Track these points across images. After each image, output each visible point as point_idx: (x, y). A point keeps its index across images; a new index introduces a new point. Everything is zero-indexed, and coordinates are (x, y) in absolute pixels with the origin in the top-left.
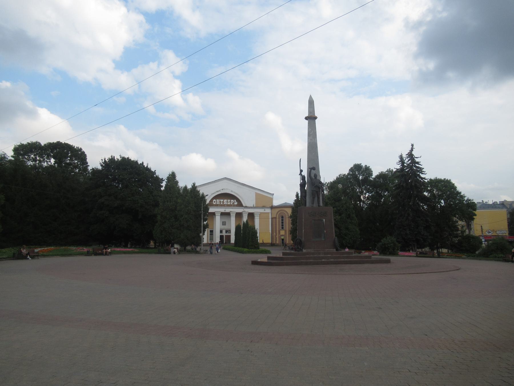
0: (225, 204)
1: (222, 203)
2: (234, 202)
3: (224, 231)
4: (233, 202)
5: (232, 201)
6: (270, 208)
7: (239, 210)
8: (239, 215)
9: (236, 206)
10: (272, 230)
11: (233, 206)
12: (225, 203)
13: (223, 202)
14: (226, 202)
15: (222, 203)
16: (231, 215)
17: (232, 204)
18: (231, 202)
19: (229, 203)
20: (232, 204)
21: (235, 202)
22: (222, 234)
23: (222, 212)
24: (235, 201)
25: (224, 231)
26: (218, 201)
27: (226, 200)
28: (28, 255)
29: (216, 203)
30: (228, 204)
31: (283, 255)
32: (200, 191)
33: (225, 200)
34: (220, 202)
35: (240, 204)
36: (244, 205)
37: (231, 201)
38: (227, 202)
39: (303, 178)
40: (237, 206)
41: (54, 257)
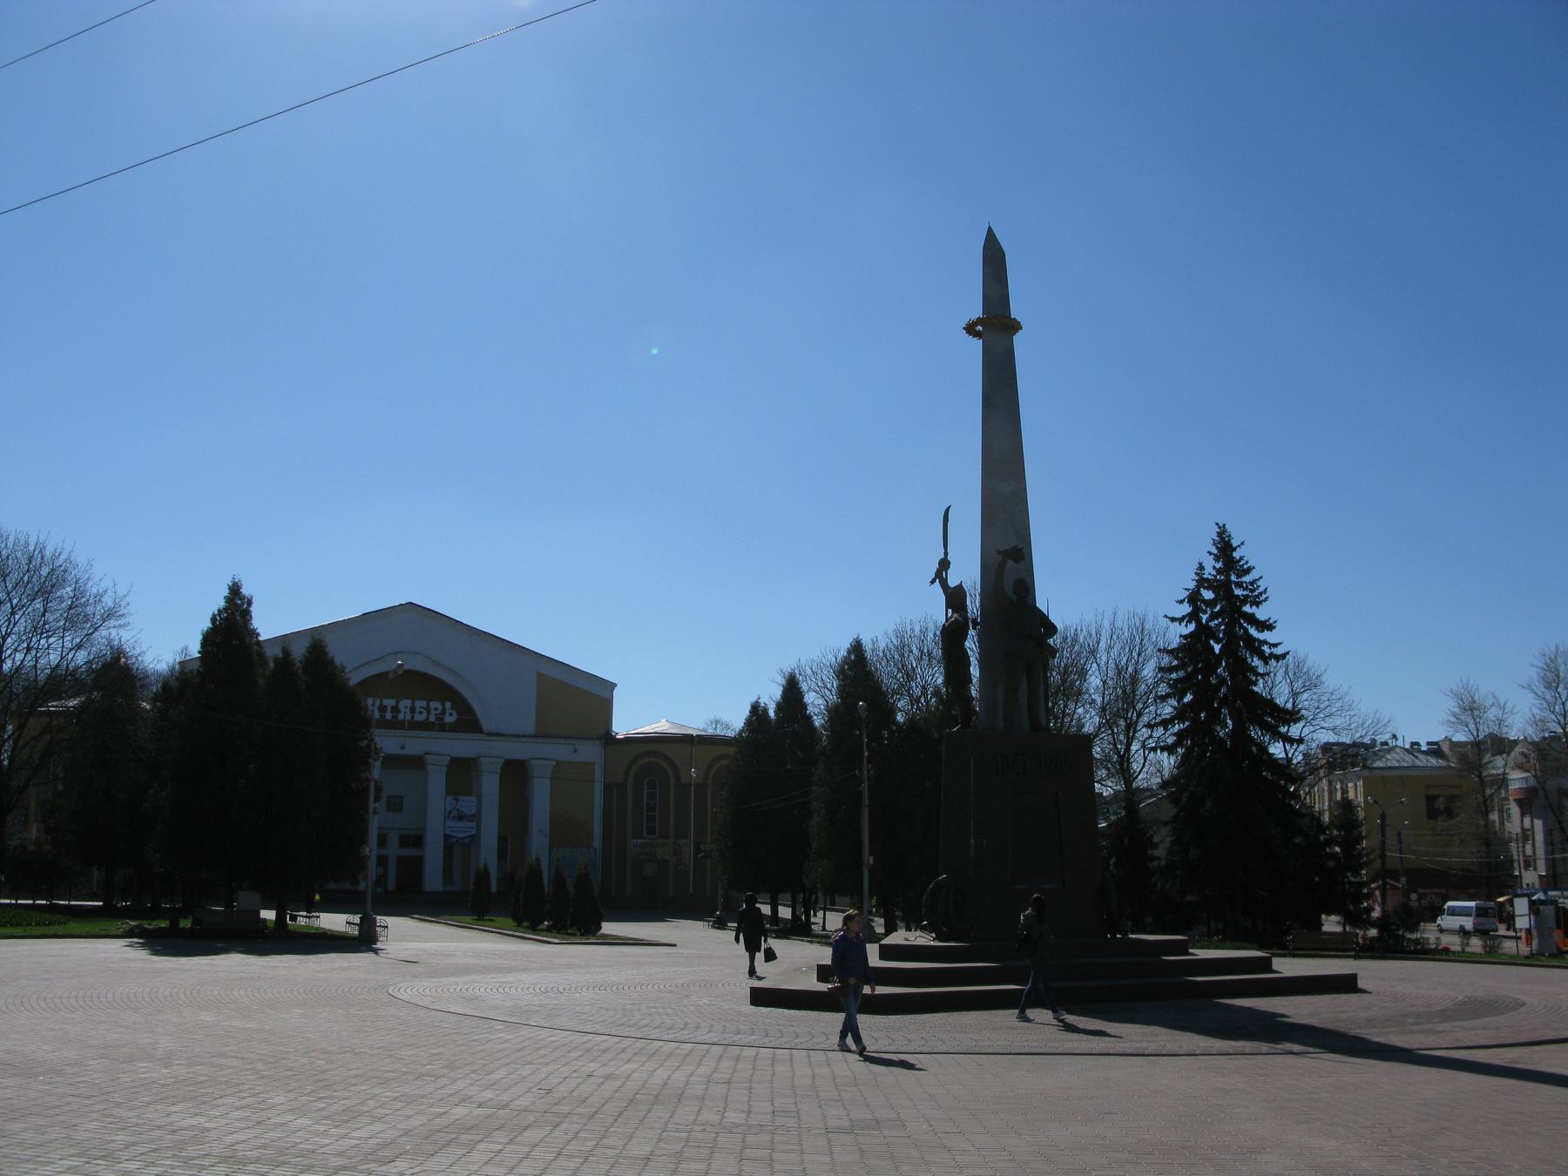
0: (401, 717)
1: (389, 716)
2: (443, 712)
3: (393, 840)
4: (436, 709)
5: (434, 705)
6: (598, 742)
7: (463, 746)
8: (462, 773)
9: (450, 731)
10: (502, 840)
11: (440, 726)
12: (404, 715)
13: (395, 710)
14: (408, 710)
15: (389, 716)
16: (430, 768)
17: (432, 719)
18: (428, 710)
19: (451, 714)
20: (432, 719)
21: (448, 711)
22: (383, 852)
23: (508, 757)
24: (448, 705)
25: (393, 840)
26: (373, 705)
27: (408, 703)
28: (1396, 933)
29: (428, 718)
30: (419, 718)
31: (882, 958)
32: (1324, 678)
33: (405, 704)
34: (383, 709)
35: (468, 723)
36: (486, 725)
37: (428, 704)
38: (413, 710)
39: (955, 598)
40: (455, 728)
41: (795, 939)
